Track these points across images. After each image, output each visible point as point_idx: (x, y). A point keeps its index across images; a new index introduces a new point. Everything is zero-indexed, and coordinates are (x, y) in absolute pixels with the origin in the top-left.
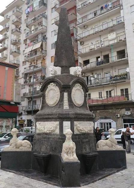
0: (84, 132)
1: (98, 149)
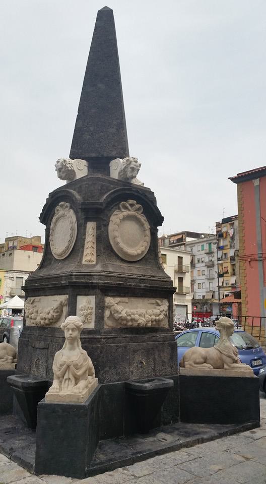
0: (135, 324)
1: (183, 371)
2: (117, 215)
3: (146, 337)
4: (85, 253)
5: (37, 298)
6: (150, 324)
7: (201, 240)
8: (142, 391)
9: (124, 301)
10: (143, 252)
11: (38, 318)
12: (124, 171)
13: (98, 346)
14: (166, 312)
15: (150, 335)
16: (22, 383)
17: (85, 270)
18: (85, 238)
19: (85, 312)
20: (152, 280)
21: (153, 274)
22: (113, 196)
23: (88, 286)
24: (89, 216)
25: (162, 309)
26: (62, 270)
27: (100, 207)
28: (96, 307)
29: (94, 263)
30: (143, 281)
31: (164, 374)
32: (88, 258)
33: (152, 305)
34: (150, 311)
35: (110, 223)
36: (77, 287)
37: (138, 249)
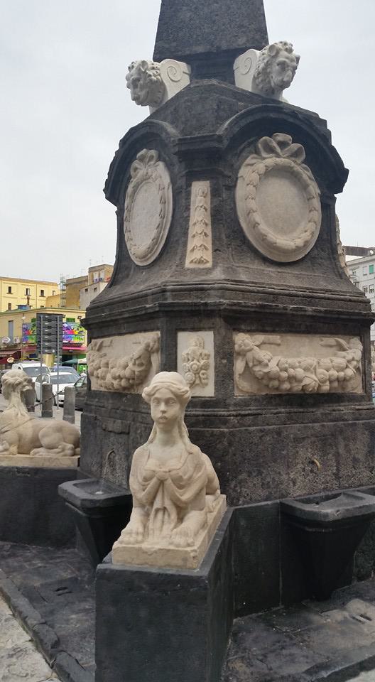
0: (297, 388)
2: (252, 165)
3: (319, 412)
4: (190, 247)
5: (107, 341)
6: (326, 387)
7: (369, 258)
8: (316, 521)
9: (271, 341)
10: (306, 243)
11: (109, 376)
12: (264, 73)
13: (223, 432)
14: (358, 362)
15: (327, 409)
16: (83, 500)
17: (189, 279)
18: (189, 216)
19: (195, 364)
20: (329, 299)
21: (330, 287)
22: (243, 123)
23: (199, 310)
24: (196, 169)
25: (350, 357)
26: (147, 284)
27: (216, 145)
28: (217, 353)
29: (209, 265)
30: (310, 299)
31: (357, 483)
32: (197, 255)
33: (329, 348)
34: (326, 361)
35: (240, 182)
36: (175, 313)
37: (297, 237)
